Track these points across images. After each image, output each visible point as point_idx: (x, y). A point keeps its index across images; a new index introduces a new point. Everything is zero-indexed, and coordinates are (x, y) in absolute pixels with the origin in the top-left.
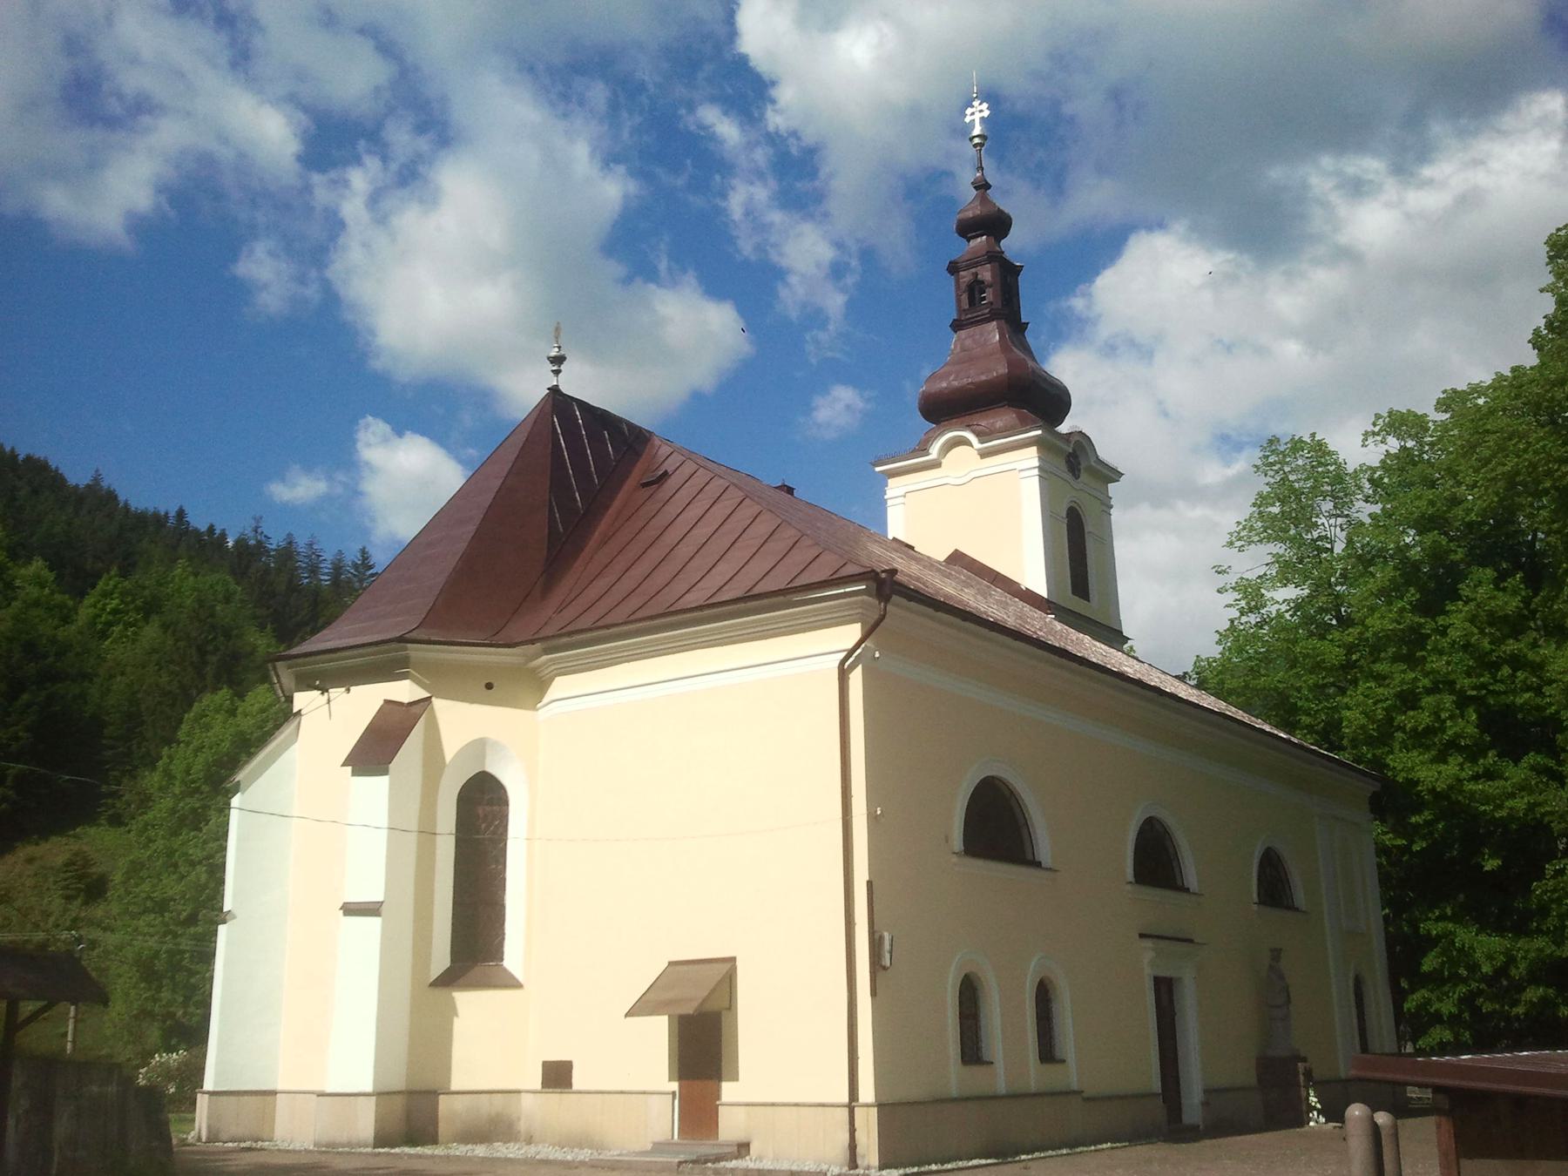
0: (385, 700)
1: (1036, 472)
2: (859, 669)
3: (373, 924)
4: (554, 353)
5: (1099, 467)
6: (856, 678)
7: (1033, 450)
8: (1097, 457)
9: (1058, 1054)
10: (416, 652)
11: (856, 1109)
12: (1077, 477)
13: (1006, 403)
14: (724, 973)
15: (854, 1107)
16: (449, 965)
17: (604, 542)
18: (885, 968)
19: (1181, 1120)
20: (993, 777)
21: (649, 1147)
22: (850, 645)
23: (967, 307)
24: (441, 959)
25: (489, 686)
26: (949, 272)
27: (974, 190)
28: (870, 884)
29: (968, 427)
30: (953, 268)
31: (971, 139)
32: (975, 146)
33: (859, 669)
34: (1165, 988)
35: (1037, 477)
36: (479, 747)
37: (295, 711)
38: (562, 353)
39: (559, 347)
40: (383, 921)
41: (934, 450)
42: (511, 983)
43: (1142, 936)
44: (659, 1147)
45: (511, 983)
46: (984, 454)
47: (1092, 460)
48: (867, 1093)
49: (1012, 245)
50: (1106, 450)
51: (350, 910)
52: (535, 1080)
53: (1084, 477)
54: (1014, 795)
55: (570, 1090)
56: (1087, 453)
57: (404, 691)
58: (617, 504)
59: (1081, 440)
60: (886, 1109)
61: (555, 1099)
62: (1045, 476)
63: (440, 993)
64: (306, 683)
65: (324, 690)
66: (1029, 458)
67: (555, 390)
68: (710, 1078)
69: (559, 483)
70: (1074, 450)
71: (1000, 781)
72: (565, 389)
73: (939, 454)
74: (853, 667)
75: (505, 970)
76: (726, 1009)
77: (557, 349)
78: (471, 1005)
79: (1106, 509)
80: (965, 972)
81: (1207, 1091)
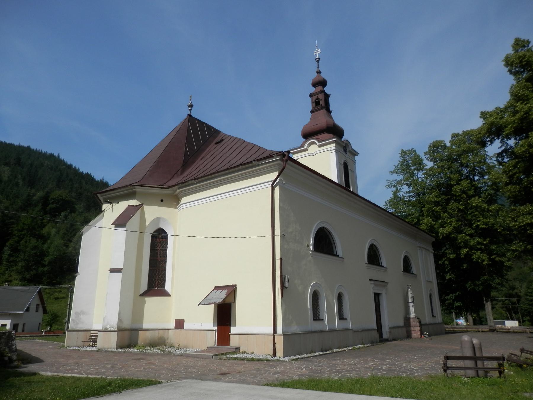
0: (129, 205)
1: (335, 151)
2: (278, 187)
3: (119, 276)
4: (189, 104)
5: (352, 151)
6: (277, 190)
7: (334, 145)
8: (352, 148)
9: (345, 317)
10: (138, 189)
11: (276, 336)
12: (346, 153)
13: (326, 132)
14: (232, 290)
15: (275, 335)
16: (147, 289)
17: (202, 159)
18: (286, 288)
19: (382, 337)
20: (323, 227)
21: (206, 348)
22: (274, 179)
23: (315, 106)
24: (144, 287)
25: (162, 201)
26: (311, 113)
27: (316, 74)
28: (281, 259)
29: (316, 139)
30: (311, 95)
31: (316, 59)
32: (317, 61)
33: (278, 187)
34: (377, 296)
35: (335, 152)
36: (158, 220)
37: (103, 210)
38: (192, 104)
39: (191, 102)
40: (122, 274)
41: (306, 147)
42: (167, 294)
43: (370, 280)
44: (210, 349)
45: (167, 294)
46: (320, 146)
47: (350, 148)
48: (280, 330)
49: (327, 90)
50: (355, 146)
51: (112, 271)
52: (172, 325)
53: (348, 153)
54: (330, 234)
55: (183, 329)
56: (348, 145)
57: (134, 202)
58: (208, 149)
59: (347, 142)
60: (285, 335)
61: (178, 332)
62: (337, 152)
63: (142, 298)
64: (107, 202)
65: (111, 203)
66: (333, 146)
67: (190, 115)
68: (227, 325)
69: (189, 141)
70: (345, 145)
71: (325, 229)
72: (193, 115)
73: (307, 147)
74: (276, 186)
75: (166, 291)
76: (233, 302)
77: (190, 103)
78: (151, 302)
79: (354, 163)
80: (314, 290)
81: (390, 328)
